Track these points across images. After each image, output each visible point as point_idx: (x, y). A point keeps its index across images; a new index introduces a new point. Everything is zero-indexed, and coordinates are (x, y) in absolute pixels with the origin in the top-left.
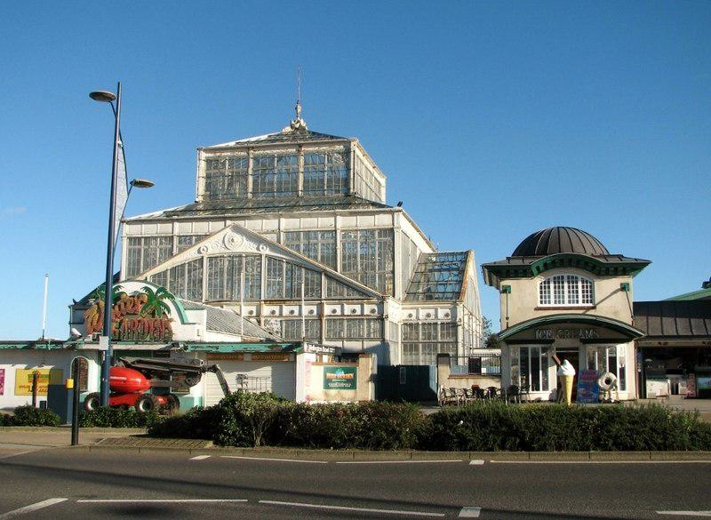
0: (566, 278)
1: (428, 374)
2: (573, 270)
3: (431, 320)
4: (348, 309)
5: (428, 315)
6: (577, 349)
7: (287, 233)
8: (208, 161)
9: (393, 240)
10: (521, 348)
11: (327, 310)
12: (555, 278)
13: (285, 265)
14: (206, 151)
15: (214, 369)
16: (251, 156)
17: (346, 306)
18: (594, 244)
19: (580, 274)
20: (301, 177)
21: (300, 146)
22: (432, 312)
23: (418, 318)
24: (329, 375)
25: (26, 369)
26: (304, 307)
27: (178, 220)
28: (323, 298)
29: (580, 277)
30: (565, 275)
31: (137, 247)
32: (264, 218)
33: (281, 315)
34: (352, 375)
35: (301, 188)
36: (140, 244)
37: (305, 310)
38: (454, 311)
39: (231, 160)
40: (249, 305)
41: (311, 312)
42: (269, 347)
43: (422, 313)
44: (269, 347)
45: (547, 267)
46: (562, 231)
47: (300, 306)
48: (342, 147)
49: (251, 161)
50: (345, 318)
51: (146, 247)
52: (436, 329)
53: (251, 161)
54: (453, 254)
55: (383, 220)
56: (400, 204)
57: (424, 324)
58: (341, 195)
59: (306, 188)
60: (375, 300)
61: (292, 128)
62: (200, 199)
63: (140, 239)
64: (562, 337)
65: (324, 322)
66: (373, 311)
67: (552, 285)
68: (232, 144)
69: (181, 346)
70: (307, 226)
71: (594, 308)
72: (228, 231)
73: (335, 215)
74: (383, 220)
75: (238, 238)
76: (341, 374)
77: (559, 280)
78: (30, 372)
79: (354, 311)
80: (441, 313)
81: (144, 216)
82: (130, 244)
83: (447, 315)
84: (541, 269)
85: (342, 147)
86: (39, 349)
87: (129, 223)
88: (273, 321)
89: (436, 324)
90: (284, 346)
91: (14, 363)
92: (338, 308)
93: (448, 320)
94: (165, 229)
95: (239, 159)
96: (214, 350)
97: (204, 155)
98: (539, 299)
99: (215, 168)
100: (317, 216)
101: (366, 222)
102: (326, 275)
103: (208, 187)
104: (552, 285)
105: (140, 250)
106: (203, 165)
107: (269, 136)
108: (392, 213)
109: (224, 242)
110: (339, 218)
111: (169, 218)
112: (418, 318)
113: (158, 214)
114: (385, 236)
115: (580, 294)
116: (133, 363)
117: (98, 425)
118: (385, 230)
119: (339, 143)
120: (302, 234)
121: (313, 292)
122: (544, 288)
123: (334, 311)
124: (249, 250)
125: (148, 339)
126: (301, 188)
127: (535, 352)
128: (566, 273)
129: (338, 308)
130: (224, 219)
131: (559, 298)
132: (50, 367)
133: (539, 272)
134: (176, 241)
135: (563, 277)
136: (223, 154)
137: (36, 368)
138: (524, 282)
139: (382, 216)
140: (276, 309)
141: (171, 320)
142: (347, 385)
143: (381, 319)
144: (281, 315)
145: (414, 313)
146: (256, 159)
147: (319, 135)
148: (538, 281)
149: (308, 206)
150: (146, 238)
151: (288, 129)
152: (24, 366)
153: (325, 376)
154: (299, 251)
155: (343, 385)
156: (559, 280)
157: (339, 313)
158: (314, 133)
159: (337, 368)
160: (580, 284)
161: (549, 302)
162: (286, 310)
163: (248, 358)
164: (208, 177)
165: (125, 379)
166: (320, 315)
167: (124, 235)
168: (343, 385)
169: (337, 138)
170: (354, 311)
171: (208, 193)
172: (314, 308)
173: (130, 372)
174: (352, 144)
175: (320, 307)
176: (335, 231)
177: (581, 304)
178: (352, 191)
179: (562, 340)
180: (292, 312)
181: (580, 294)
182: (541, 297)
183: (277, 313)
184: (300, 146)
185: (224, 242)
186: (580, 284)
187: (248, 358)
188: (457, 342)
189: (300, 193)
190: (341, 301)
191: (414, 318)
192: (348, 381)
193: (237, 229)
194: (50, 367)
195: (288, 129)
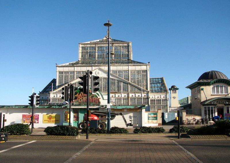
0: (219, 86)
1: (164, 115)
2: (221, 83)
3: (159, 98)
4: (137, 95)
5: (158, 97)
6: (223, 107)
7: (131, 71)
8: (82, 47)
9: (147, 74)
10: (205, 107)
11: (130, 95)
12: (216, 86)
13: (116, 81)
14: (82, 44)
15: (121, 114)
16: (97, 46)
17: (136, 94)
18: (223, 75)
19: (223, 85)
20: (97, 54)
21: (113, 44)
22: (159, 96)
23: (155, 98)
24: (149, 115)
25: (46, 114)
26: (142, 94)
27: (76, 66)
28: (129, 91)
29: (223, 86)
30: (219, 85)
31: (62, 75)
32: (105, 66)
33: (115, 97)
34: (156, 115)
35: (97, 57)
36: (63, 74)
37: (123, 95)
38: (166, 96)
39: (90, 47)
40: (124, 94)
41: (125, 96)
42: (134, 107)
43: (156, 97)
44: (134, 107)
45: (214, 83)
46: (213, 72)
47: (141, 94)
48: (126, 44)
49: (97, 48)
50: (136, 98)
51: (119, 74)
52: (160, 101)
53: (97, 48)
54: (156, 78)
55: (144, 68)
56: (149, 63)
57: (157, 100)
58: (126, 59)
59: (98, 58)
60: (146, 92)
61: (106, 38)
62: (80, 60)
63: (63, 72)
64: (219, 103)
65: (129, 99)
66: (145, 96)
67: (215, 88)
68: (89, 42)
69: (104, 107)
70: (120, 69)
71: (228, 95)
72: (97, 70)
73: (128, 66)
74: (144, 68)
75: (100, 72)
76: (153, 115)
77: (217, 87)
78: (48, 116)
79: (54, 96)
80: (162, 97)
81: (64, 65)
82: (59, 74)
83: (164, 97)
84: (213, 83)
85: (126, 44)
86: (53, 108)
87: (59, 67)
88: (113, 99)
89: (161, 100)
90: (139, 106)
91: (42, 113)
92: (134, 95)
93: (164, 98)
94: (71, 69)
95: (93, 47)
96: (116, 108)
97: (81, 46)
98: (212, 92)
99: (84, 50)
100: (123, 66)
101: (138, 68)
102: (130, 84)
103: (82, 56)
104: (215, 88)
105: (63, 76)
106: (81, 49)
107: (90, 42)
108: (146, 65)
109: (96, 74)
110: (129, 67)
111: (73, 65)
112: (155, 98)
113: (68, 64)
114: (144, 72)
115: (224, 91)
116: (93, 112)
117: (143, 132)
118: (144, 71)
119: (126, 43)
120: (64, 72)
121: (126, 90)
122: (213, 89)
123: (133, 96)
124: (104, 76)
125: (92, 104)
126: (97, 57)
127: (209, 108)
128: (220, 84)
129: (134, 95)
130: (92, 66)
131: (218, 92)
132: (55, 114)
133: (212, 84)
134: (75, 73)
135: (218, 86)
136: (87, 46)
137: (50, 114)
138: (207, 87)
139: (143, 66)
140: (114, 95)
141: (100, 98)
142: (154, 119)
143: (148, 98)
144: (115, 97)
145: (154, 96)
146: (98, 47)
147: (117, 41)
148: (212, 87)
149: (116, 63)
150: (124, 71)
151: (105, 38)
152: (46, 114)
153: (148, 116)
154: (122, 78)
155: (153, 119)
156: (217, 87)
157: (134, 96)
158: (114, 40)
159: (151, 113)
160: (224, 88)
161: (219, 93)
162: (117, 95)
163: (125, 110)
164: (82, 53)
165: (92, 117)
166: (128, 97)
167: (57, 71)
168: (153, 119)
169: (124, 42)
170: (139, 96)
171: (82, 58)
172: (126, 95)
173: (94, 116)
174: (130, 44)
175: (128, 94)
176: (128, 71)
177: (224, 94)
178: (130, 58)
179: (219, 104)
180: (119, 96)
181: (224, 91)
182: (212, 92)
183: (114, 96)
184: (113, 44)
185: (96, 74)
186: (224, 88)
187: (125, 110)
188: (167, 105)
189: (96, 59)
190: (135, 93)
191: (154, 98)
192: (155, 117)
193: (100, 70)
194: (55, 114)
195: (105, 38)
